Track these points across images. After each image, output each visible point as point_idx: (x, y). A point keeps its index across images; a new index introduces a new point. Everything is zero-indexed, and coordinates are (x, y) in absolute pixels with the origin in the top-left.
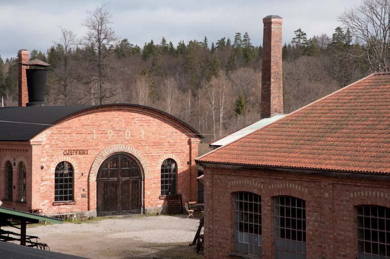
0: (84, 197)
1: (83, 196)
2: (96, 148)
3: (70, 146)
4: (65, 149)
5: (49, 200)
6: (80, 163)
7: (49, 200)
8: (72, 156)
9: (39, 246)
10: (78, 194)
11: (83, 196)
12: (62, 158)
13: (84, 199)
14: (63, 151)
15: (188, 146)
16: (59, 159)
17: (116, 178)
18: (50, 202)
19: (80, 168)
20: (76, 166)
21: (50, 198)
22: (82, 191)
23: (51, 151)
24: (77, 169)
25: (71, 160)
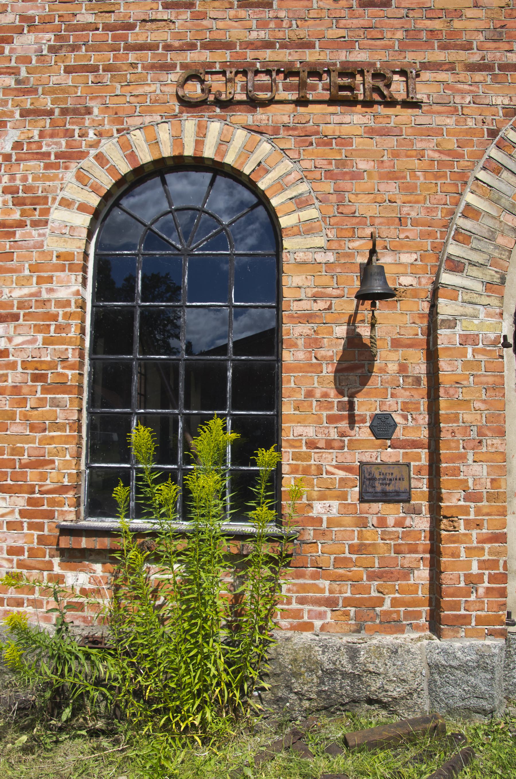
0: (386, 498)
1: (377, 487)
2: (496, 56)
3: (236, 33)
4: (190, 57)
5: (20, 501)
6: (341, 173)
7: (20, 501)
8: (261, 117)
9: (361, 98)
10: (328, 459)
11: (377, 487)
12: (164, 133)
13: (392, 512)
14: (174, 77)
15: (376, 106)
16: (138, 138)
17: (297, 79)
18: (33, 513)
19: (343, 219)
20: (300, 203)
21: (32, 476)
22: (363, 432)
23: (59, 78)
24: (306, 229)
25: (248, 151)
